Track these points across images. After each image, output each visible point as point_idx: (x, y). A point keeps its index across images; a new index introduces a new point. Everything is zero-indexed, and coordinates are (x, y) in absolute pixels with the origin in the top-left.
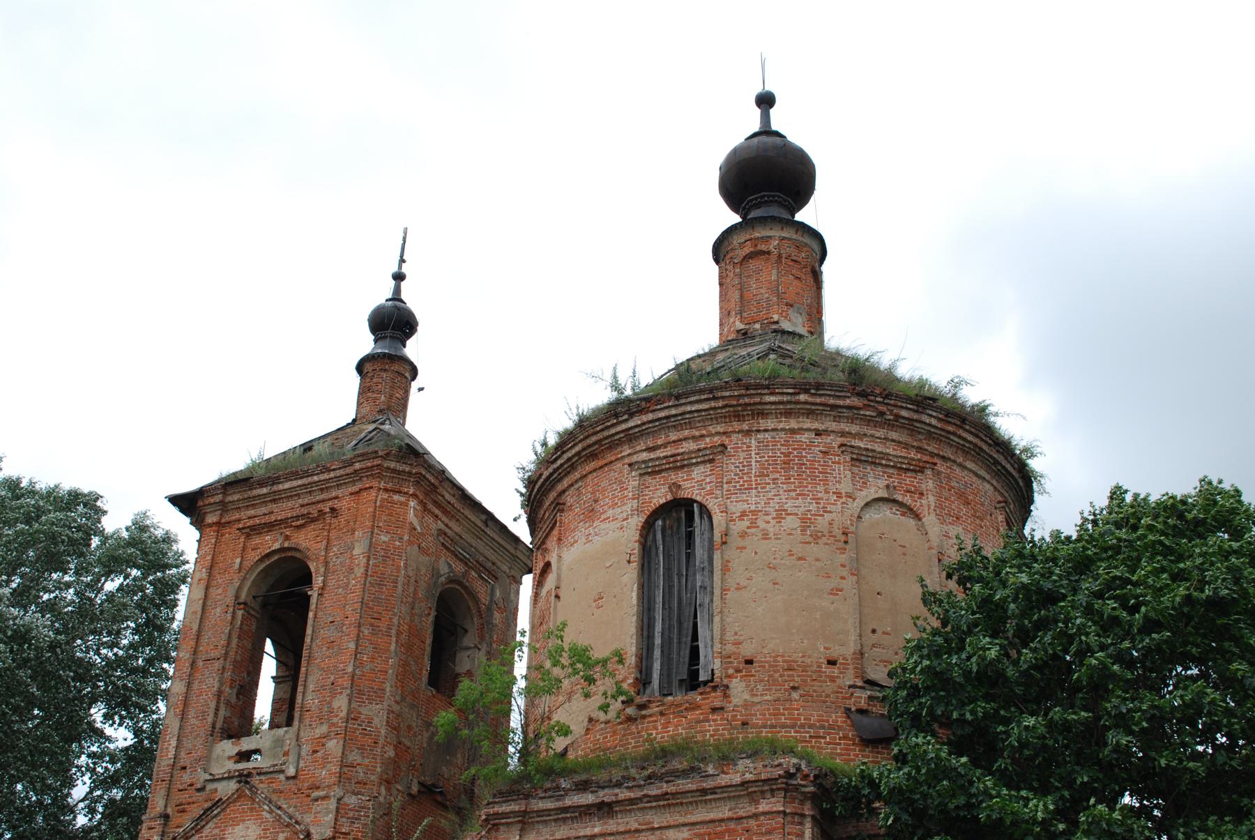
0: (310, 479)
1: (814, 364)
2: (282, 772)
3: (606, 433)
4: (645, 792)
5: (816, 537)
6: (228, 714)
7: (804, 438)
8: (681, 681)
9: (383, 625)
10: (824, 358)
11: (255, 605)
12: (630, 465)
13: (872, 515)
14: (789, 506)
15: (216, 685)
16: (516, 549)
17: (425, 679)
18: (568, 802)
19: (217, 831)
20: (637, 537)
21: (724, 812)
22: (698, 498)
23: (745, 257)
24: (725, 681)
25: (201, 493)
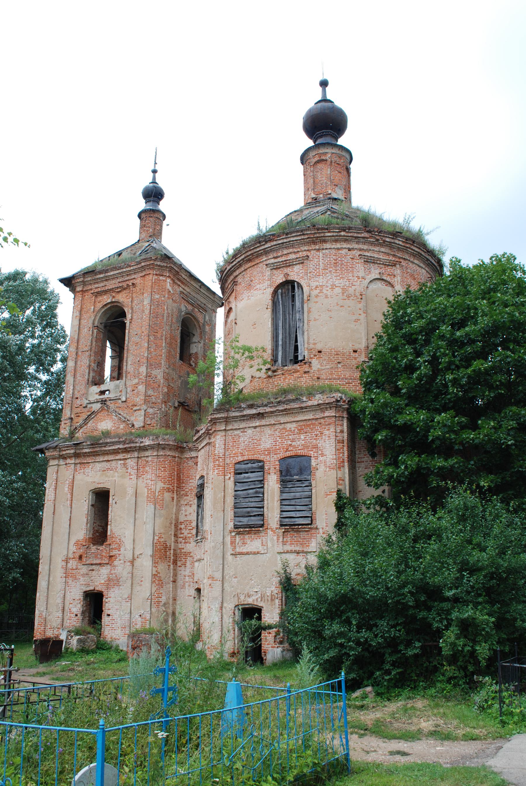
0: (122, 270)
1: (347, 216)
2: (120, 399)
3: (255, 250)
4: (277, 408)
5: (349, 297)
6: (94, 375)
7: (343, 252)
8: (291, 360)
9: (159, 335)
10: (352, 212)
11: (102, 327)
12: (266, 265)
13: (373, 286)
14: (337, 283)
15: (88, 363)
16: (214, 297)
17: (178, 357)
18: (245, 413)
19: (94, 424)
20: (270, 297)
21: (310, 416)
22: (297, 280)
23: (315, 162)
24: (310, 360)
25: (73, 277)
